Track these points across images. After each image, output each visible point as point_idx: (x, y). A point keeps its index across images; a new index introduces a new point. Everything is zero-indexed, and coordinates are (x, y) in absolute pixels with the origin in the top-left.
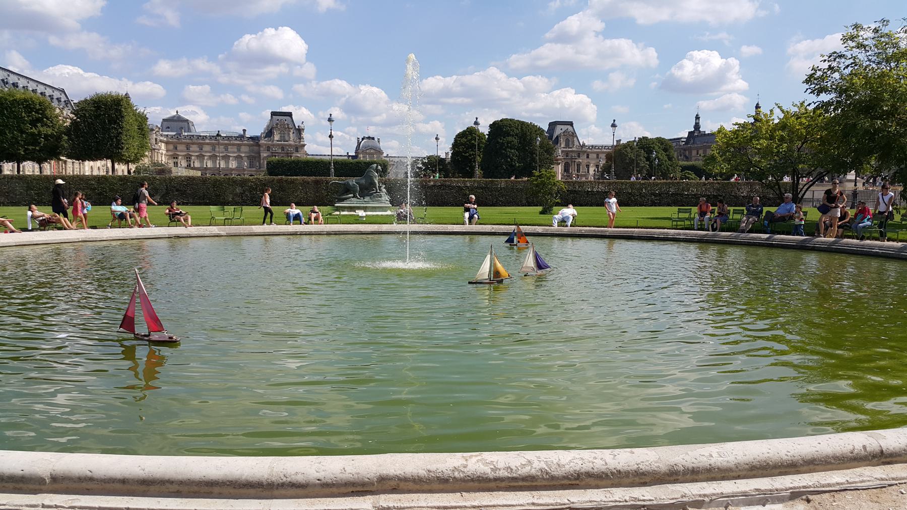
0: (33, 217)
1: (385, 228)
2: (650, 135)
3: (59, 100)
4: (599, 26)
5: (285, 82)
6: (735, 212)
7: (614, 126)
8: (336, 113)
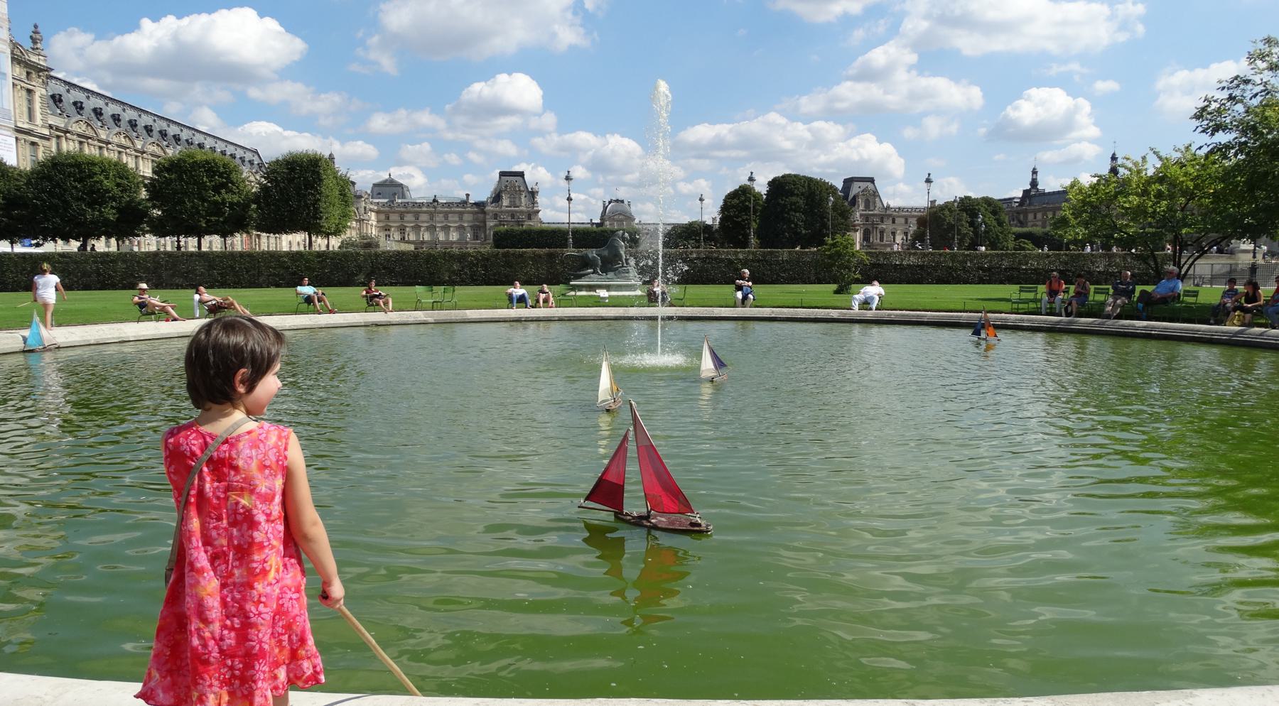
0: (201, 302)
1: (633, 311)
2: (973, 196)
3: (251, 162)
4: (912, 58)
5: (521, 137)
6: (1097, 292)
7: (928, 181)
8: (579, 172)
